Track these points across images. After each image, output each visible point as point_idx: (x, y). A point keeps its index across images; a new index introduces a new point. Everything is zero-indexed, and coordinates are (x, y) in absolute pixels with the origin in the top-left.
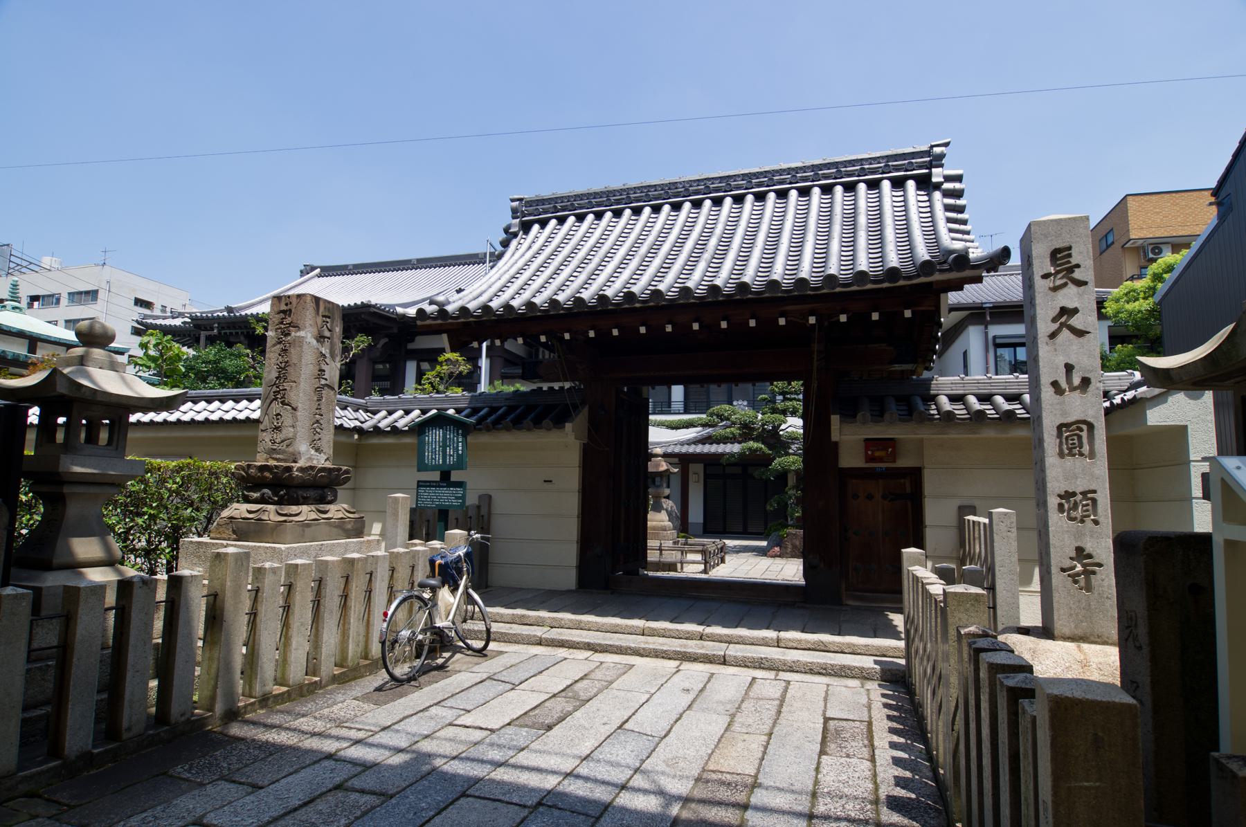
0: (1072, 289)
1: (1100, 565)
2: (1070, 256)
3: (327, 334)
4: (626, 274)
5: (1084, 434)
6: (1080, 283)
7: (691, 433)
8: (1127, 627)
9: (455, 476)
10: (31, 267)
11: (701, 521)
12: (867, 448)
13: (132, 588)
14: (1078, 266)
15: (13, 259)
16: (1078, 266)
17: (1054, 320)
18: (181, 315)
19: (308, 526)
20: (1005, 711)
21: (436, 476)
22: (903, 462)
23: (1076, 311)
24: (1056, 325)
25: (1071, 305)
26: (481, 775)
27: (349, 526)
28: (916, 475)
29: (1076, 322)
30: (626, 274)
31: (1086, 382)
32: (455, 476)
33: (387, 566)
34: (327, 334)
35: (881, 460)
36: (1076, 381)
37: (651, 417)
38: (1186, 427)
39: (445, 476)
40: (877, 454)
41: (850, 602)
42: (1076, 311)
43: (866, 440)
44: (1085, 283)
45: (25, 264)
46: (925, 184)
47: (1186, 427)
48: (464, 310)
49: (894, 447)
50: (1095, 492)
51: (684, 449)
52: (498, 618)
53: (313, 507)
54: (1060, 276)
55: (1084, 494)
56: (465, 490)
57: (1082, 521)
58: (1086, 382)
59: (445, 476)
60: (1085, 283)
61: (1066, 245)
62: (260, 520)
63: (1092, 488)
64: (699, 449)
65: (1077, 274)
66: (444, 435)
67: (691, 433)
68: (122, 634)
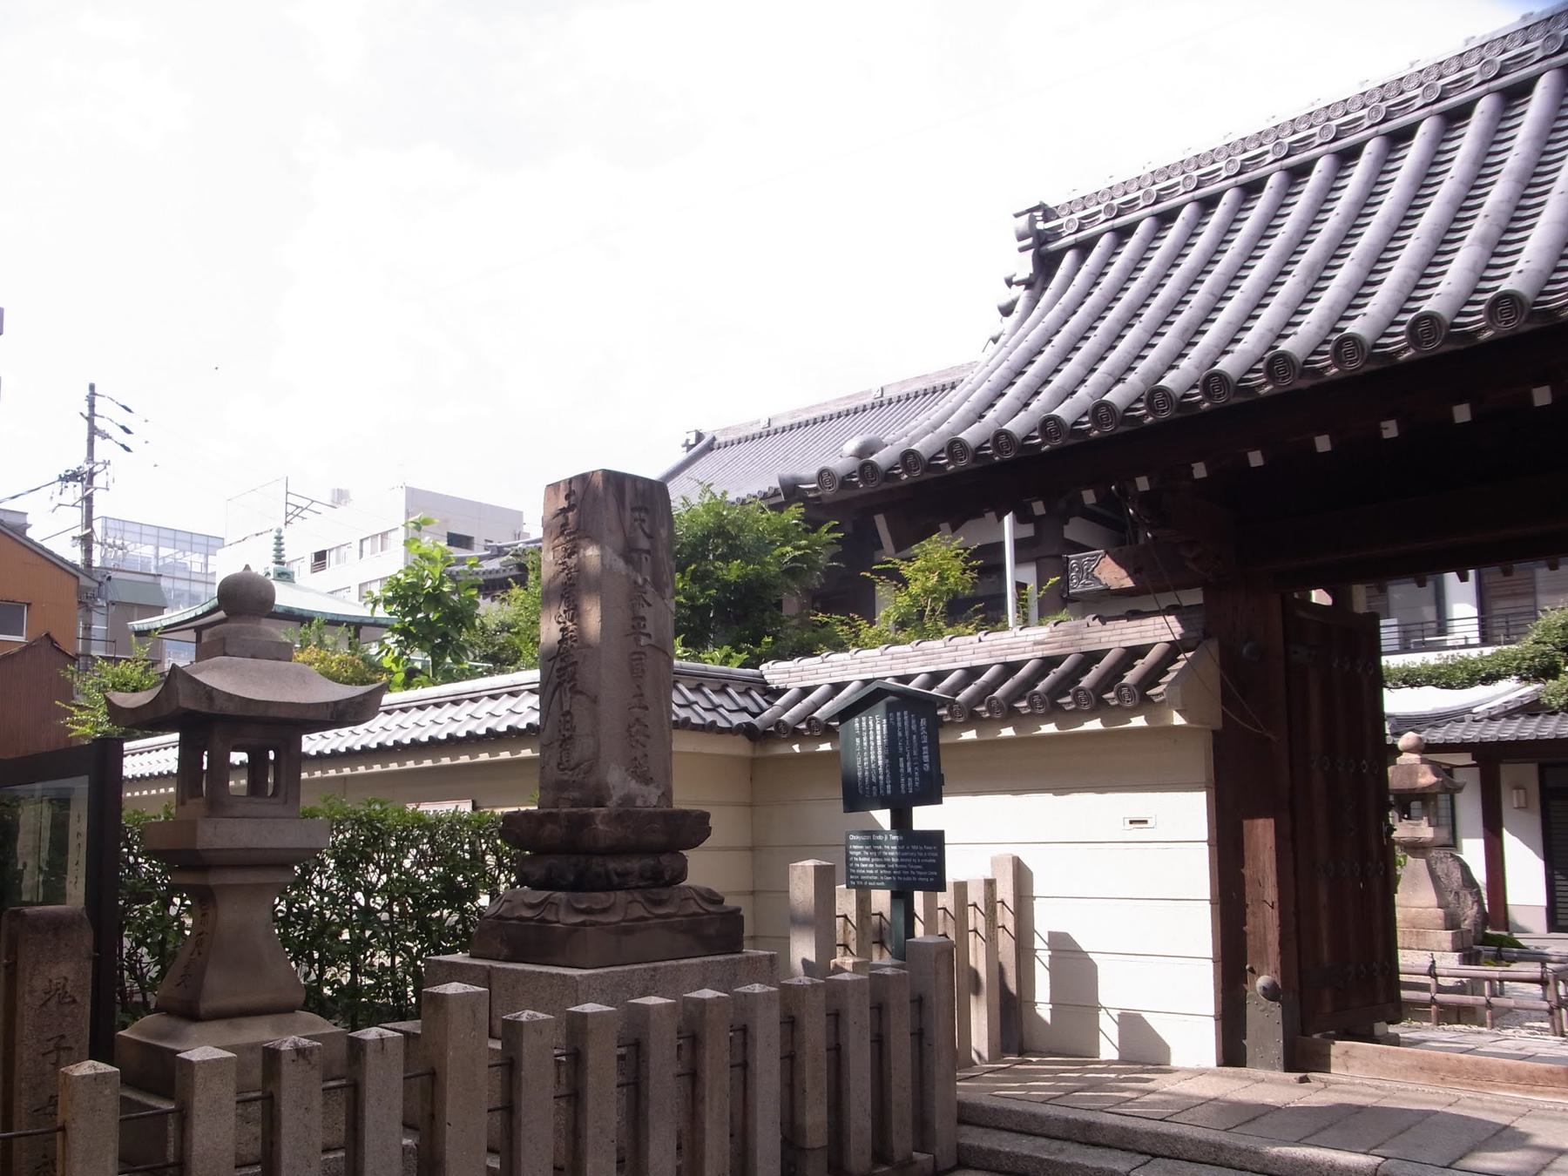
3: (644, 543)
4: (1268, 317)
7: (1509, 691)
10: (315, 507)
11: (1542, 900)
13: (279, 1059)
15: (291, 499)
18: (500, 552)
19: (628, 931)
26: (1507, 1123)
27: (711, 931)
30: (1268, 317)
33: (775, 1014)
34: (644, 543)
37: (1390, 662)
38: (942, 833)
45: (304, 503)
47: (942, 833)
48: (909, 458)
51: (1493, 732)
52: (1034, 1127)
53: (637, 895)
62: (543, 920)
64: (1529, 729)
67: (1509, 691)
68: (272, 1144)
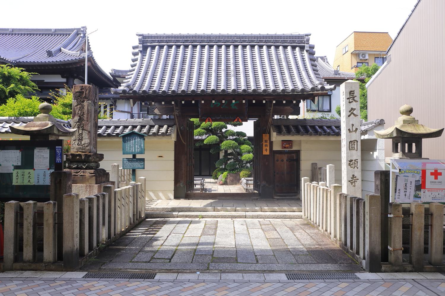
0: (354, 103)
1: (358, 179)
2: (354, 93)
5: (356, 144)
6: (356, 101)
8: (348, 99)
9: (138, 156)
12: (283, 144)
14: (356, 96)
16: (356, 96)
17: (350, 112)
20: (85, 242)
21: (131, 156)
22: (295, 148)
23: (355, 109)
24: (350, 113)
25: (354, 108)
28: (298, 152)
29: (355, 112)
31: (357, 129)
32: (138, 156)
35: (287, 148)
36: (354, 129)
39: (134, 156)
40: (286, 146)
41: (276, 197)
42: (355, 109)
43: (282, 141)
44: (358, 101)
46: (302, 48)
49: (292, 143)
50: (357, 160)
54: (351, 99)
55: (355, 160)
56: (144, 162)
57: (354, 168)
58: (357, 129)
59: (134, 156)
60: (358, 101)
61: (353, 90)
63: (357, 159)
65: (355, 99)
66: (251, 184)
